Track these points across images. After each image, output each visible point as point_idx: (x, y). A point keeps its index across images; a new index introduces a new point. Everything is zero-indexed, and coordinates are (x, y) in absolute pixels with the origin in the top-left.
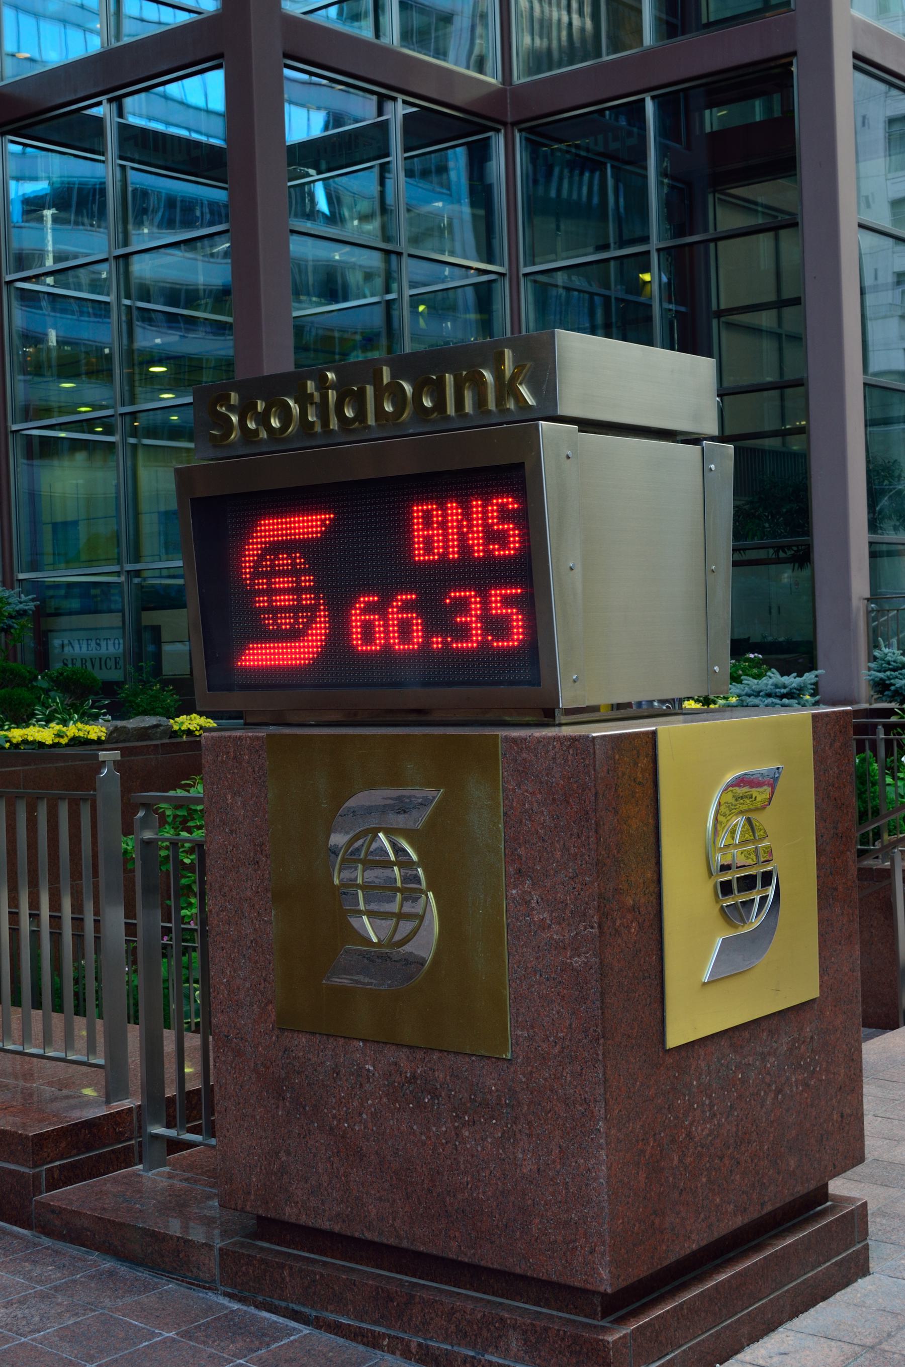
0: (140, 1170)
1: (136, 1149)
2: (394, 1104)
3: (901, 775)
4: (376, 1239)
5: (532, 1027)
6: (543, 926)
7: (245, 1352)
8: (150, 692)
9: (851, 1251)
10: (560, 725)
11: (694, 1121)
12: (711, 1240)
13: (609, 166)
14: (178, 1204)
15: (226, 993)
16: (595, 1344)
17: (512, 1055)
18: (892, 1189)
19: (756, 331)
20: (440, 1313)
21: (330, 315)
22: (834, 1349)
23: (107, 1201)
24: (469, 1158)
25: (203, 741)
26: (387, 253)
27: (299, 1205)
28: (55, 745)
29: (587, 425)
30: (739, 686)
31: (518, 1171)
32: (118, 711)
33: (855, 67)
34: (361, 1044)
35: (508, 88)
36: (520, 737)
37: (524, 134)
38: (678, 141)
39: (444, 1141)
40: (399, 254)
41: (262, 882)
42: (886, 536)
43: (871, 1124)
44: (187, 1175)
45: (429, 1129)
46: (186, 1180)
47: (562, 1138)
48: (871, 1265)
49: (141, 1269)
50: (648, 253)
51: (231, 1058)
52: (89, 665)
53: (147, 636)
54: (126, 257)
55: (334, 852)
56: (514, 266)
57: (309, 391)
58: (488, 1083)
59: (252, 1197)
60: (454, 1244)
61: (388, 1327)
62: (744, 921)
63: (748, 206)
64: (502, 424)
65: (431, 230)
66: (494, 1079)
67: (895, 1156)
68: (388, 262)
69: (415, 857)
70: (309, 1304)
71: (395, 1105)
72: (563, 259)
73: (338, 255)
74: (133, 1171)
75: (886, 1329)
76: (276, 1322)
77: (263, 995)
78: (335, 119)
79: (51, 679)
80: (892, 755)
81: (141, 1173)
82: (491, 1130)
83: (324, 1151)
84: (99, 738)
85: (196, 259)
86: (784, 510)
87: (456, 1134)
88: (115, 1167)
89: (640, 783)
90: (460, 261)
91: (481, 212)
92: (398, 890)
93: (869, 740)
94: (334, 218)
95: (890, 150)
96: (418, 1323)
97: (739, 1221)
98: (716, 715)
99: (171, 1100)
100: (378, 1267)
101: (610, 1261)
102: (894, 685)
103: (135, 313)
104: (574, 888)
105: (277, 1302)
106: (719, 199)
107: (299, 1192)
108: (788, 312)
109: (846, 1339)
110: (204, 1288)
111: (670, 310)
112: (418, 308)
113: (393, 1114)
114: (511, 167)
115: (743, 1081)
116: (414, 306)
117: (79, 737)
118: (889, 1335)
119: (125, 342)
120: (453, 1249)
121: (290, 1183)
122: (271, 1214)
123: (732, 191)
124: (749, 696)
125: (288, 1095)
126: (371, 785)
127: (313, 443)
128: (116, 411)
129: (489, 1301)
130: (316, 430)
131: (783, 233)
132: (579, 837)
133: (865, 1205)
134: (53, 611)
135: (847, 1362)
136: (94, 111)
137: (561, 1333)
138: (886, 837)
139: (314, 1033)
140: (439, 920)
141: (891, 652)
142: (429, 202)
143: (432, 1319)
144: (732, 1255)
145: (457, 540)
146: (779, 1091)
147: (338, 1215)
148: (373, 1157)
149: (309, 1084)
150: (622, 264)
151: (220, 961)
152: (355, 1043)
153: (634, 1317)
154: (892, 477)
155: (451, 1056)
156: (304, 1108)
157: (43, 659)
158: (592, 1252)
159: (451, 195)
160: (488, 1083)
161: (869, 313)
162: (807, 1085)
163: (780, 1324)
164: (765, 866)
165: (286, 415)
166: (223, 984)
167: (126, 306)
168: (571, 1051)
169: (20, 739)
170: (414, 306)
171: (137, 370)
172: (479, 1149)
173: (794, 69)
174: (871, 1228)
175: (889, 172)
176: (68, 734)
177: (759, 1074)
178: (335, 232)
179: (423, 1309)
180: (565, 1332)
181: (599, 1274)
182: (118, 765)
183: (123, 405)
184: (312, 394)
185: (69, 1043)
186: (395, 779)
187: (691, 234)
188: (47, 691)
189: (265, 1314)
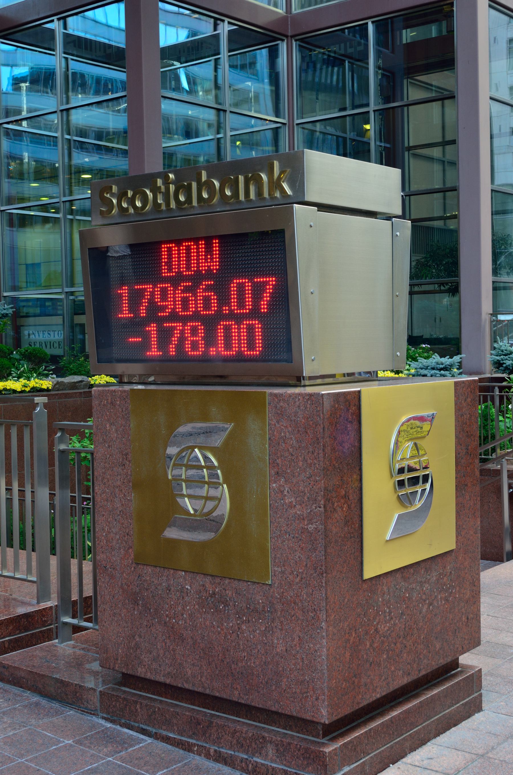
0: (56, 643)
1: (54, 631)
2: (202, 609)
3: (508, 416)
4: (191, 688)
5: (284, 566)
6: (291, 506)
7: (113, 753)
9: (471, 697)
10: (305, 386)
11: (379, 622)
12: (388, 691)
13: (347, 62)
14: (78, 664)
15: (105, 541)
16: (318, 753)
17: (272, 582)
18: (496, 660)
20: (227, 733)
23: (36, 661)
24: (246, 642)
25: (93, 392)
26: (218, 110)
27: (146, 667)
28: (22, 392)
29: (323, 207)
30: (416, 363)
31: (274, 650)
32: (60, 372)
33: (490, 6)
34: (183, 573)
36: (279, 393)
37: (298, 42)
38: (387, 48)
39: (231, 632)
40: (225, 111)
41: (127, 477)
43: (486, 620)
44: (84, 646)
45: (222, 624)
46: (83, 649)
47: (300, 631)
48: (483, 705)
49: (54, 702)
50: (368, 112)
51: (107, 580)
52: (44, 345)
53: (77, 329)
54: (67, 110)
55: (170, 458)
57: (158, 185)
58: (257, 598)
59: (119, 662)
60: (236, 693)
61: (197, 740)
62: (411, 504)
63: (427, 86)
65: (243, 99)
67: (499, 640)
68: (218, 116)
69: (216, 464)
70: (151, 725)
71: (203, 610)
72: (320, 115)
73: (191, 112)
74: (53, 643)
75: (491, 745)
76: (132, 735)
77: (126, 543)
79: (21, 354)
80: (503, 404)
81: (57, 644)
82: (259, 626)
83: (161, 636)
84: (48, 388)
85: (109, 114)
87: (239, 628)
88: (42, 641)
91: (274, 88)
92: (206, 483)
94: (192, 91)
95: (509, 55)
96: (214, 738)
97: (405, 681)
98: (403, 381)
99: (75, 602)
100: (192, 704)
101: (328, 705)
103: (72, 142)
104: (310, 484)
105: (133, 723)
106: (410, 82)
107: (146, 660)
109: (467, 750)
110: (91, 714)
111: (381, 146)
113: (202, 615)
115: (410, 598)
116: (233, 142)
117: (37, 387)
118: (493, 748)
122: (130, 672)
124: (422, 369)
126: (191, 420)
127: (161, 216)
128: (60, 200)
129: (256, 726)
130: (162, 208)
131: (446, 102)
132: (313, 453)
133: (481, 669)
134: (25, 314)
135: (467, 764)
136: (48, 26)
137: (298, 746)
138: (498, 451)
140: (230, 501)
141: (504, 344)
143: (223, 736)
144: (401, 700)
145: (185, 264)
146: (430, 604)
147: (169, 673)
148: (189, 640)
149: (153, 596)
150: (353, 119)
151: (102, 523)
152: (180, 573)
153: (342, 737)
154: (507, 244)
155: (236, 582)
156: (150, 610)
157: (18, 342)
158: (317, 699)
159: (258, 80)
160: (257, 598)
161: (495, 151)
162: (447, 600)
163: (429, 740)
164: (425, 472)
165: (145, 200)
166: (103, 536)
167: (67, 139)
168: (306, 580)
169: (2, 388)
171: (73, 176)
172: (252, 637)
174: (484, 683)
176: (30, 385)
177: (419, 594)
179: (217, 730)
180: (300, 746)
181: (321, 712)
182: (45, 406)
184: (160, 187)
185: (16, 567)
186: (205, 418)
187: (394, 102)
188: (19, 361)
189: (126, 730)
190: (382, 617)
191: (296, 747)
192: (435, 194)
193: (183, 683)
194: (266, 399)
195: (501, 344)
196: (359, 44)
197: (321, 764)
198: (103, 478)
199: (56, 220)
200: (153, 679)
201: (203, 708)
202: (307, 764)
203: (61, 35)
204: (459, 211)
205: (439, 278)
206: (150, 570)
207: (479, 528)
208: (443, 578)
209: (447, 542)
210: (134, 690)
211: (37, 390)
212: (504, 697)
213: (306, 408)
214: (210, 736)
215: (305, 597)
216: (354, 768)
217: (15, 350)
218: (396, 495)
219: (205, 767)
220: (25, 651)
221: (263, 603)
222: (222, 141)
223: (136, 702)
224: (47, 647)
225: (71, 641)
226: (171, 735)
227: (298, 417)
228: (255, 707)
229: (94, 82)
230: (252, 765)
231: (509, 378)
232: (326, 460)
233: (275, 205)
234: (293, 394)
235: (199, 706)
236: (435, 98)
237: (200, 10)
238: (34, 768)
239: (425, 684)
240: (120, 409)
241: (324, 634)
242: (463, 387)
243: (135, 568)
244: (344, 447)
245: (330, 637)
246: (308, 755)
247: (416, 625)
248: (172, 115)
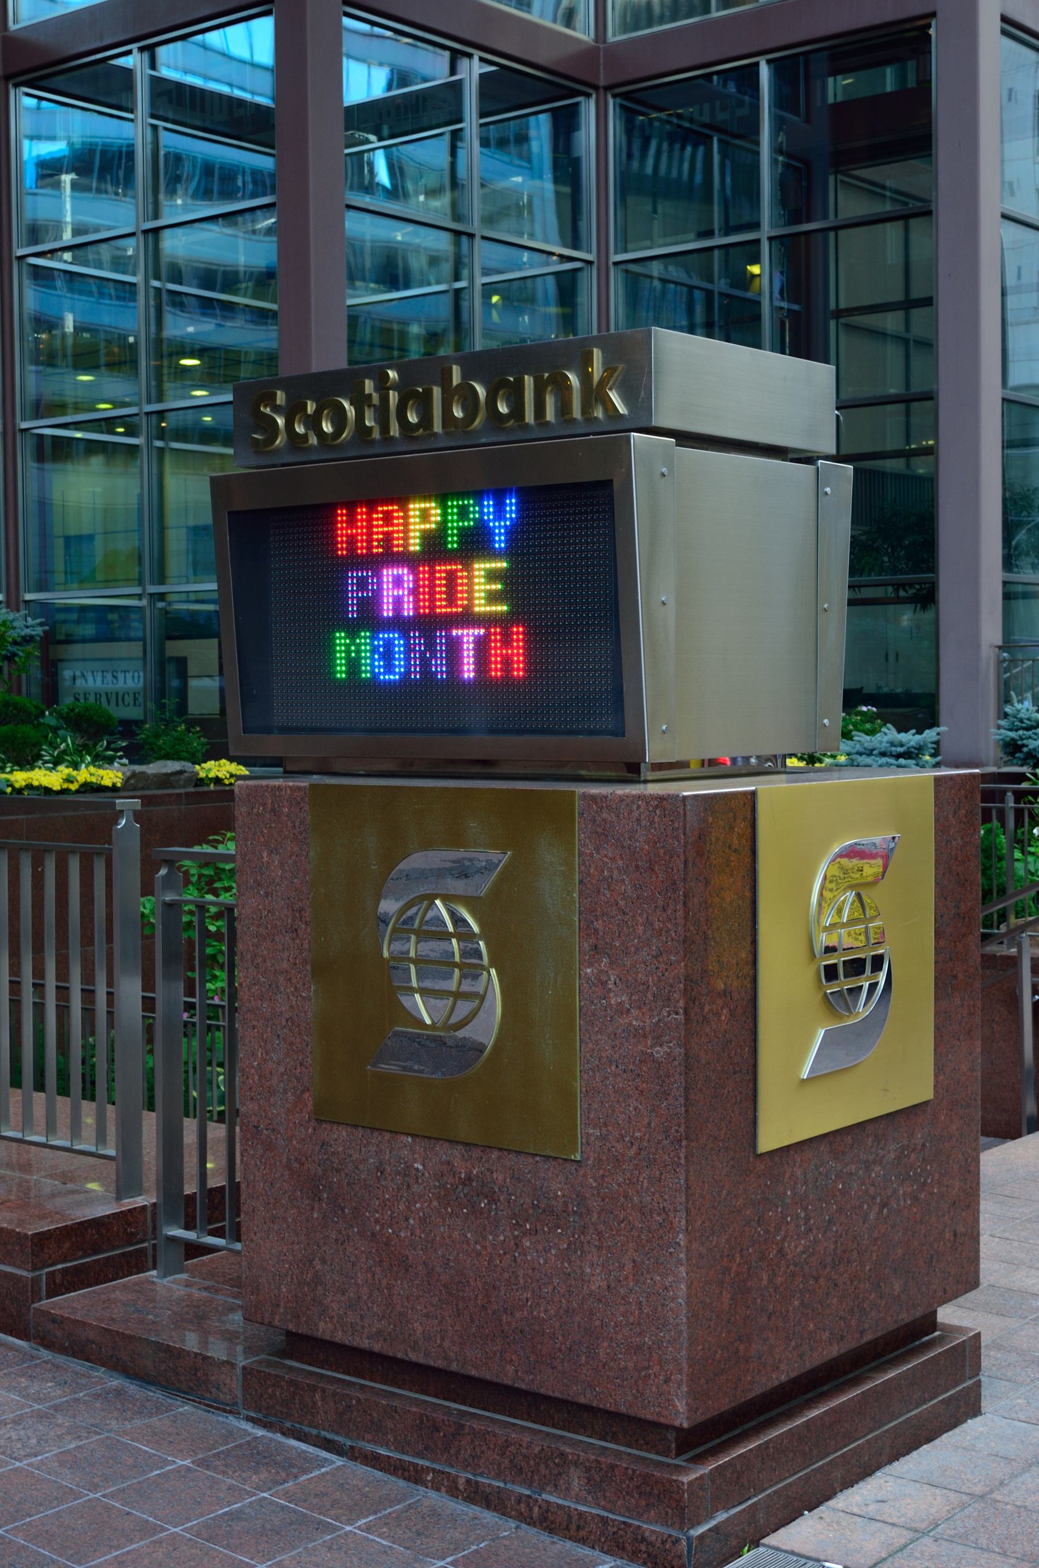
0: (153, 1276)
1: (150, 1253)
2: (446, 1208)
3: (1032, 849)
4: (422, 1361)
5: (606, 1125)
6: (622, 1011)
8: (175, 734)
9: (960, 1388)
10: (646, 782)
12: (803, 1371)
13: (715, 140)
14: (197, 1316)
16: (667, 1485)
17: (582, 1157)
18: (1009, 1320)
19: (879, 335)
20: (492, 1446)
24: (530, 1271)
25: (237, 791)
26: (457, 233)
27: (335, 1320)
28: (63, 792)
29: (686, 438)
30: (849, 742)
31: (585, 1287)
32: (136, 754)
34: (410, 1139)
37: (618, 100)
38: (797, 113)
39: (501, 1252)
40: (471, 236)
41: (301, 953)
42: (1022, 575)
43: (987, 1245)
44: (207, 1283)
45: (485, 1238)
47: (636, 1251)
49: (153, 1388)
50: (757, 242)
51: (260, 1152)
52: (104, 699)
53: (171, 669)
54: (156, 231)
55: (384, 920)
56: (603, 252)
57: (367, 392)
58: (553, 1187)
59: (282, 1310)
61: (433, 1461)
63: (875, 190)
64: (588, 435)
66: (560, 1183)
68: (457, 244)
69: (476, 929)
70: (343, 1432)
71: (446, 1210)
73: (400, 234)
76: (305, 1452)
78: (400, 77)
79: (60, 716)
80: (1023, 826)
81: (155, 1279)
83: (364, 1260)
84: (114, 785)
86: (907, 542)
87: (516, 1244)
89: (735, 851)
92: (456, 965)
94: (396, 192)
97: (834, 1351)
99: (191, 1199)
101: (687, 1392)
103: (165, 297)
104: (657, 968)
105: (307, 1429)
106: (842, 182)
107: (335, 1306)
108: (916, 313)
109: (953, 1487)
110: (225, 1411)
111: (782, 308)
112: (490, 298)
113: (444, 1220)
116: (487, 295)
117: (92, 782)
123: (856, 173)
124: (860, 754)
126: (427, 845)
127: (371, 452)
128: (141, 409)
129: (548, 1434)
131: (913, 222)
133: (978, 1336)
135: (953, 1513)
136: (121, 62)
137: (630, 1471)
138: (1012, 920)
139: (356, 1126)
141: (1025, 708)
144: (825, 1388)
146: (884, 1205)
147: (379, 1332)
148: (420, 1268)
149: (349, 1184)
150: (727, 254)
151: (250, 1042)
152: (403, 1138)
153: (713, 1456)
155: (512, 1156)
156: (343, 1211)
157: (51, 692)
160: (553, 1187)
161: (1010, 317)
162: (915, 1199)
165: (339, 418)
166: (253, 1067)
167: (155, 288)
169: (24, 784)
170: (487, 295)
171: (166, 363)
172: (542, 1261)
174: (985, 1363)
176: (79, 778)
178: (395, 208)
179: (472, 1441)
180: (634, 1471)
181: (675, 1406)
183: (149, 402)
184: (370, 395)
186: (456, 839)
187: (808, 221)
188: (55, 730)
190: (792, 1227)
191: (625, 1474)
192: (888, 407)
193: (406, 1351)
194: (574, 806)
195: (1019, 706)
196: (741, 104)
197: (674, 1504)
198: (255, 956)
199: (132, 450)
200: (347, 1343)
201: (445, 1399)
202: (647, 1505)
203: (146, 80)
204: (937, 440)
205: (895, 574)
206: (344, 1133)
207: (980, 1061)
208: (908, 1156)
209: (919, 1088)
210: (310, 1364)
211: (92, 788)
212: (1023, 1390)
213: (652, 822)
214: (458, 1452)
215: (645, 1184)
216: (735, 1514)
217: (48, 707)
218: (821, 994)
219: (448, 1512)
220: (94, 1292)
221: (564, 1196)
222: (465, 295)
223: (314, 1389)
224: (136, 1284)
225: (182, 1273)
226: (382, 1452)
227: (637, 840)
228: (546, 1398)
229: (198, 172)
230: (540, 1507)
231: (1035, 775)
232: (689, 923)
233: (594, 434)
234: (627, 797)
235: (436, 1396)
236: (892, 215)
237: (422, 31)
238: (118, 1510)
239: (874, 1359)
240: (289, 823)
241: (682, 1256)
242: (951, 789)
243: (314, 1129)
244: (723, 899)
245: (694, 1261)
246: (648, 1489)
247: (855, 1245)
248: (363, 241)
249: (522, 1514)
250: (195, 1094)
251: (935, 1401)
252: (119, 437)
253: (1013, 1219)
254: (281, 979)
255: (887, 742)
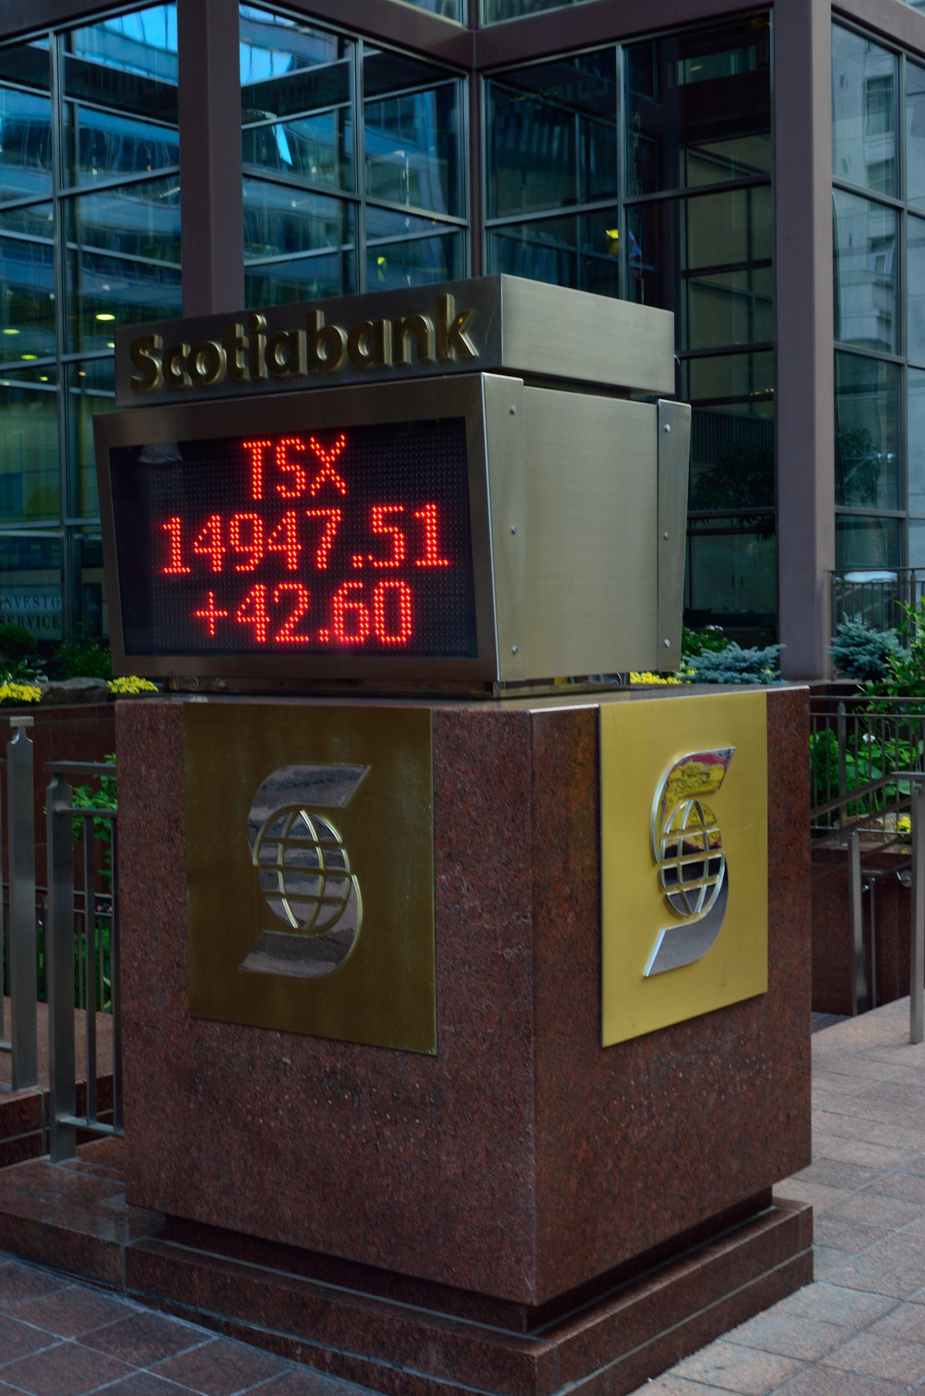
0: (46, 1160)
1: (44, 1138)
3: (862, 754)
4: (291, 1242)
6: (474, 914)
8: (89, 653)
10: (499, 699)
14: (86, 1198)
17: (438, 1052)
19: (725, 293)
20: (356, 1322)
21: (284, 265)
22: (773, 1364)
25: (117, 709)
26: (345, 201)
29: (533, 378)
31: (442, 1174)
32: (55, 671)
33: (834, 21)
34: (279, 1035)
35: (474, 32)
36: (453, 712)
37: (489, 81)
39: (364, 1141)
40: (357, 203)
42: (853, 508)
43: (819, 1120)
47: (488, 1140)
49: (43, 1268)
50: (615, 208)
52: (26, 622)
54: (73, 198)
55: (256, 826)
56: (476, 218)
59: (161, 1195)
61: (302, 1335)
63: (720, 163)
64: (441, 375)
65: (390, 181)
66: (418, 1076)
68: (345, 211)
69: (338, 838)
76: (183, 1327)
78: (299, 61)
80: (854, 733)
81: (49, 1164)
84: (33, 700)
86: (750, 479)
87: (378, 1134)
89: (581, 764)
90: (425, 214)
91: (445, 162)
92: (320, 872)
93: (830, 717)
94: (298, 166)
97: (676, 1228)
99: (82, 1087)
102: (857, 661)
103: (80, 256)
105: (185, 1306)
108: (758, 273)
109: (787, 1353)
110: (110, 1289)
111: (637, 269)
112: (376, 261)
114: (475, 114)
116: (372, 258)
117: (13, 698)
119: (69, 287)
120: (372, 1256)
121: (201, 1181)
122: (181, 1213)
123: (705, 147)
124: (708, 668)
125: (201, 1088)
126: (293, 759)
128: (58, 359)
129: (408, 1311)
132: (513, 820)
133: (810, 1210)
135: (786, 1378)
136: (37, 44)
138: (844, 817)
139: (229, 1023)
142: (391, 150)
144: (668, 1262)
146: (722, 1091)
156: (217, 1102)
158: (518, 1261)
161: (842, 280)
163: (718, 1334)
165: (212, 361)
167: (71, 250)
170: (372, 258)
171: (81, 317)
172: (401, 1149)
173: (771, 25)
174: (817, 1232)
175: (867, 135)
178: (291, 180)
180: (488, 1346)
181: (525, 1285)
182: (30, 731)
183: (66, 352)
184: (240, 339)
186: (319, 755)
200: (222, 1225)
201: (313, 1277)
203: (62, 61)
204: (776, 388)
206: (218, 1030)
209: (751, 981)
212: (852, 1258)
215: (497, 1077)
218: (661, 897)
221: (421, 1088)
222: (352, 257)
226: (255, 1327)
230: (401, 1380)
233: (447, 374)
237: (313, 18)
240: (166, 740)
241: (531, 1145)
243: (190, 1025)
245: (543, 1149)
249: (384, 1385)
250: (108, 982)
251: (770, 1272)
252: (42, 383)
253: (844, 1095)
254: (159, 885)
255: (732, 658)
